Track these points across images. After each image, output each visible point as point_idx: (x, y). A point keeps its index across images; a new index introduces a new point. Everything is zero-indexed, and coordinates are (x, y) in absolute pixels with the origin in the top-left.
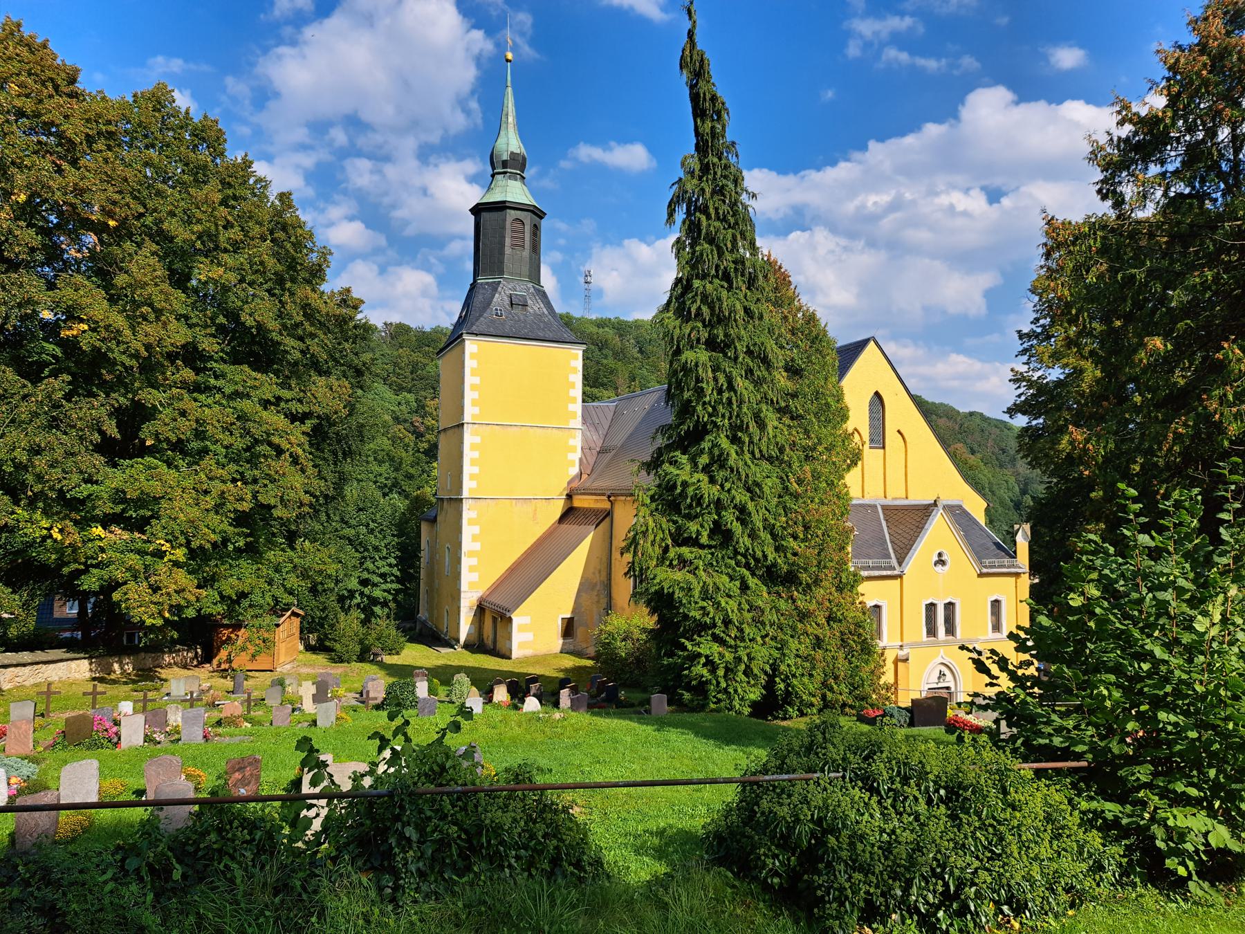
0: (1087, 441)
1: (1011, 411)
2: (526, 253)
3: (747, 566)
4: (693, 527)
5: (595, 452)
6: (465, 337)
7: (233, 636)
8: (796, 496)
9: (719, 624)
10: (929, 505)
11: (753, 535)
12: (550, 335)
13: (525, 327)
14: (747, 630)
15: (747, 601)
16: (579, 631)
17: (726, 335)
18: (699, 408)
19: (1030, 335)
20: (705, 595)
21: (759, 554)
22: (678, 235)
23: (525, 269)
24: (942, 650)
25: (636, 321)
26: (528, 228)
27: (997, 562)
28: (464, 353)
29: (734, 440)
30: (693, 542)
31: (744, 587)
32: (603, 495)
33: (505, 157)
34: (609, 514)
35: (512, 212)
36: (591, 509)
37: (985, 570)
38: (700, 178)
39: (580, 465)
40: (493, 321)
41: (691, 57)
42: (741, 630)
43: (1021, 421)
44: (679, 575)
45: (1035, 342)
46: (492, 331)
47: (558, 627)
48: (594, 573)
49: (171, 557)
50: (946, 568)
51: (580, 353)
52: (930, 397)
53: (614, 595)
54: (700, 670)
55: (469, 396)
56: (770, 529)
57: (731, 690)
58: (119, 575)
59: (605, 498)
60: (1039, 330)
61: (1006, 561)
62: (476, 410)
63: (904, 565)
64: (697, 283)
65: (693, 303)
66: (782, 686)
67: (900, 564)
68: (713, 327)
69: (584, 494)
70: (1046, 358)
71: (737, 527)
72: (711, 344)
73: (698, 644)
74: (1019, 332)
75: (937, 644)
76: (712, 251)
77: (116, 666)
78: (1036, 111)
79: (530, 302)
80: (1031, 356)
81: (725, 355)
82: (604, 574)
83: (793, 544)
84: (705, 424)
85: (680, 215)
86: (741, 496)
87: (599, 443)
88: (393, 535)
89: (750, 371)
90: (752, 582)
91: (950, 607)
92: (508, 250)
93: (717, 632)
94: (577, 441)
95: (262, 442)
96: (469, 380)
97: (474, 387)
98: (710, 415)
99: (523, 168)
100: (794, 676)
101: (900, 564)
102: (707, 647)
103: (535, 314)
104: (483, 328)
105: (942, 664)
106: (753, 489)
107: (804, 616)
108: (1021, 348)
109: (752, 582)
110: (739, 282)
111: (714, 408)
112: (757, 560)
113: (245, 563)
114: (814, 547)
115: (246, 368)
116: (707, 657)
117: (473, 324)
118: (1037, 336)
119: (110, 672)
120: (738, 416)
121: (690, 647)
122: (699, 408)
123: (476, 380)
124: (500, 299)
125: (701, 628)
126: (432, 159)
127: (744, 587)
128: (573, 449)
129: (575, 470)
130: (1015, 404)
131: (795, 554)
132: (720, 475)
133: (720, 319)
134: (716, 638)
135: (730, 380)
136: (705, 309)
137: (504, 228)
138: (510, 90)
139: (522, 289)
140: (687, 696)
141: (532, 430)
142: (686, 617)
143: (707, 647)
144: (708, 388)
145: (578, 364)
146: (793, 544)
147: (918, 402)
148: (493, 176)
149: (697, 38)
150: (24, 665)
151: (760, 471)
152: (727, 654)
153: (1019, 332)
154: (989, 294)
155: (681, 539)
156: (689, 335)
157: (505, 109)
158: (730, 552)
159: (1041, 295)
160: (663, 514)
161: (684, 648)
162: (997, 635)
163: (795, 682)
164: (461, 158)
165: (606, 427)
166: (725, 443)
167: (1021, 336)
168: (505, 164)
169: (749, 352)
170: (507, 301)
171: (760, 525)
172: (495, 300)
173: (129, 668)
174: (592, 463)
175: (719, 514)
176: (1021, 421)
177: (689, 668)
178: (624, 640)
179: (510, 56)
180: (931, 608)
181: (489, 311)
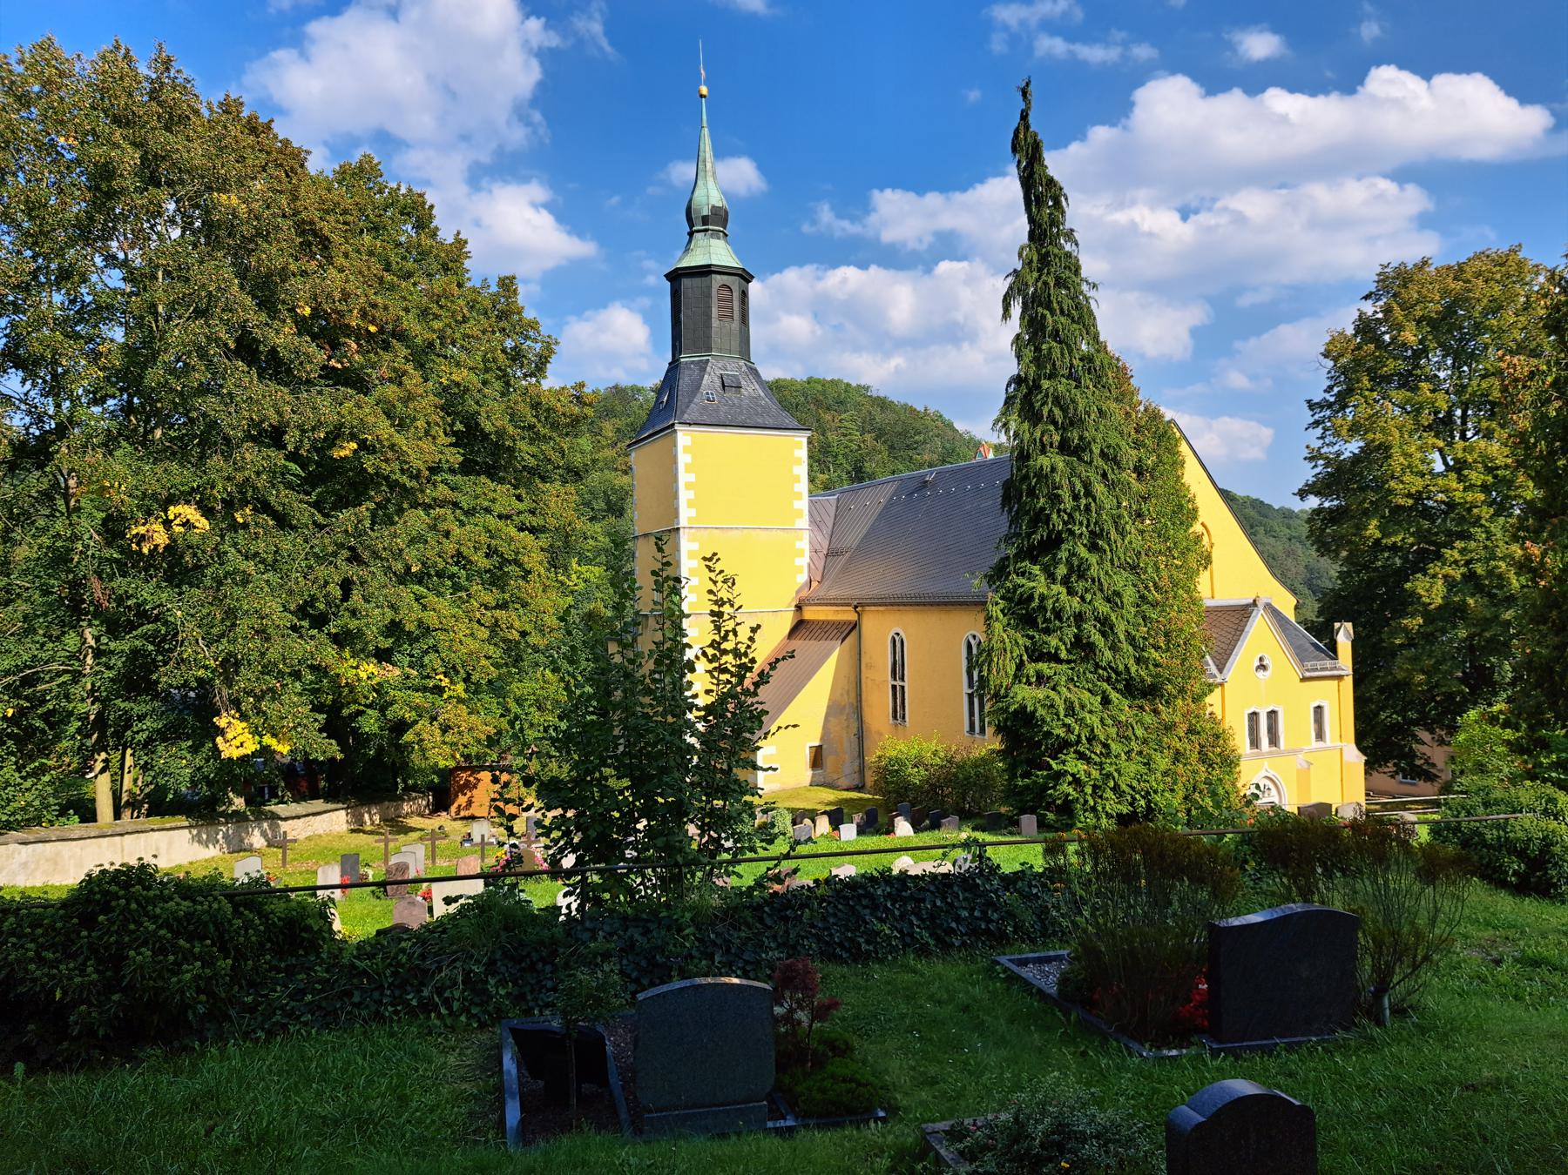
0: (1544, 554)
1: (1302, 494)
2: (736, 325)
3: (1108, 680)
4: (1053, 641)
5: (822, 555)
6: (677, 427)
7: (471, 779)
8: (1154, 605)
9: (1084, 740)
10: (1248, 606)
11: (1114, 648)
12: (770, 422)
13: (741, 413)
14: (1113, 746)
15: (1112, 718)
16: (829, 761)
17: (1081, 438)
18: (1054, 516)
19: (1322, 405)
20: (1070, 710)
21: (1121, 667)
22: (1018, 330)
23: (735, 344)
24: (1266, 763)
25: (777, 381)
26: (736, 295)
27: (1319, 664)
28: (675, 446)
29: (1093, 547)
30: (1055, 658)
31: (1106, 701)
32: (848, 605)
33: (705, 212)
34: (855, 626)
35: (718, 277)
36: (828, 622)
37: (1308, 674)
38: (1040, 270)
39: (809, 571)
40: (705, 408)
41: (1026, 139)
42: (1106, 746)
43: (1313, 502)
44: (1041, 693)
45: (1328, 412)
46: (705, 418)
47: (806, 757)
48: (842, 695)
49: (451, 693)
50: (1267, 673)
51: (805, 441)
52: (1240, 491)
53: (867, 717)
54: (1065, 788)
55: (684, 496)
56: (1131, 639)
57: (1100, 808)
58: (409, 716)
59: (850, 608)
60: (1332, 399)
61: (1328, 663)
62: (692, 512)
63: (1225, 671)
64: (1045, 384)
65: (1042, 405)
66: (1142, 803)
67: (1221, 671)
68: (1064, 429)
69: (816, 605)
70: (1344, 432)
71: (1097, 638)
72: (1064, 447)
73: (1064, 762)
74: (1309, 401)
75: (1261, 756)
76: (1062, 349)
77: (366, 816)
78: (1233, 103)
79: (743, 383)
80: (1325, 429)
81: (1080, 459)
82: (853, 695)
83: (1155, 655)
84: (1060, 533)
85: (1016, 309)
86: (1103, 608)
87: (825, 544)
88: (587, 660)
89: (1104, 475)
90: (1114, 696)
91: (1272, 715)
92: (715, 323)
93: (1082, 750)
94: (803, 544)
95: (509, 562)
96: (684, 477)
97: (689, 486)
98: (1065, 523)
99: (724, 222)
100: (1156, 792)
101: (1221, 671)
102: (1074, 766)
103: (751, 398)
104: (695, 417)
105: (1267, 777)
106: (1113, 599)
107: (1169, 728)
108: (1312, 420)
109: (1114, 696)
110: (1087, 380)
111: (1070, 515)
112: (1118, 673)
113: (487, 698)
114: (1177, 657)
115: (483, 479)
116: (1073, 775)
117: (683, 412)
118: (1330, 405)
119: (362, 823)
120: (1095, 524)
121: (1054, 766)
122: (1054, 516)
123: (691, 477)
124: (710, 381)
125: (1064, 745)
126: (484, 182)
127: (1106, 701)
128: (801, 554)
129: (803, 578)
130: (1307, 485)
131: (1156, 665)
132: (1080, 586)
133: (1074, 422)
134: (1081, 756)
135: (1087, 485)
136: (1057, 411)
137: (709, 296)
138: (706, 131)
139: (734, 368)
140: (1051, 816)
141: (754, 533)
142: (1049, 734)
143: (1074, 766)
144: (1065, 494)
145: (802, 453)
146: (1155, 655)
147: (1226, 496)
148: (691, 234)
149: (1031, 119)
150: (298, 817)
151: (1120, 580)
152: (1094, 772)
153: (1309, 401)
154: (1196, 333)
155: (1037, 654)
156: (1041, 440)
157: (701, 154)
158: (1090, 667)
159: (1335, 360)
160: (1016, 628)
161: (1049, 767)
162: (1321, 744)
163: (1157, 798)
164: (524, 180)
165: (830, 525)
166: (1083, 552)
167: (1311, 406)
168: (705, 220)
169: (1103, 455)
170: (718, 383)
171: (1122, 637)
172: (704, 382)
173: (377, 818)
174: (821, 568)
175: (1078, 627)
176: (1313, 502)
177: (1054, 788)
178: (915, 766)
179: (704, 90)
180: (1254, 716)
181: (699, 395)
